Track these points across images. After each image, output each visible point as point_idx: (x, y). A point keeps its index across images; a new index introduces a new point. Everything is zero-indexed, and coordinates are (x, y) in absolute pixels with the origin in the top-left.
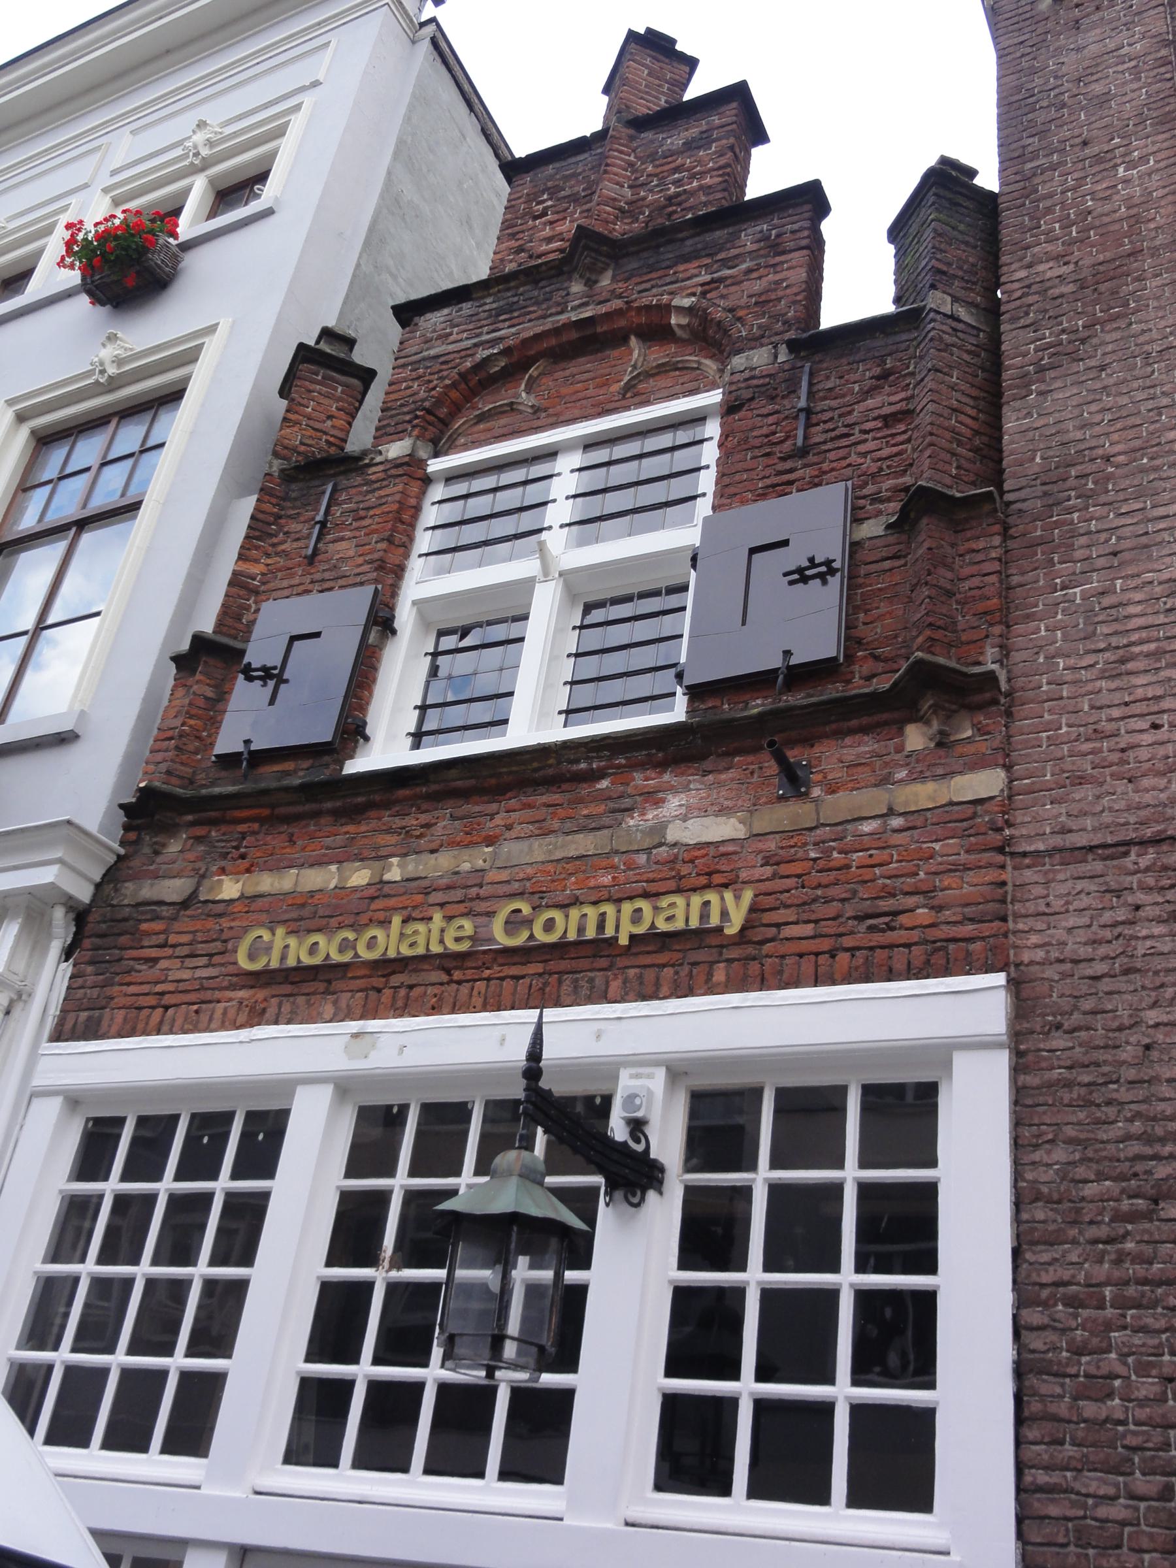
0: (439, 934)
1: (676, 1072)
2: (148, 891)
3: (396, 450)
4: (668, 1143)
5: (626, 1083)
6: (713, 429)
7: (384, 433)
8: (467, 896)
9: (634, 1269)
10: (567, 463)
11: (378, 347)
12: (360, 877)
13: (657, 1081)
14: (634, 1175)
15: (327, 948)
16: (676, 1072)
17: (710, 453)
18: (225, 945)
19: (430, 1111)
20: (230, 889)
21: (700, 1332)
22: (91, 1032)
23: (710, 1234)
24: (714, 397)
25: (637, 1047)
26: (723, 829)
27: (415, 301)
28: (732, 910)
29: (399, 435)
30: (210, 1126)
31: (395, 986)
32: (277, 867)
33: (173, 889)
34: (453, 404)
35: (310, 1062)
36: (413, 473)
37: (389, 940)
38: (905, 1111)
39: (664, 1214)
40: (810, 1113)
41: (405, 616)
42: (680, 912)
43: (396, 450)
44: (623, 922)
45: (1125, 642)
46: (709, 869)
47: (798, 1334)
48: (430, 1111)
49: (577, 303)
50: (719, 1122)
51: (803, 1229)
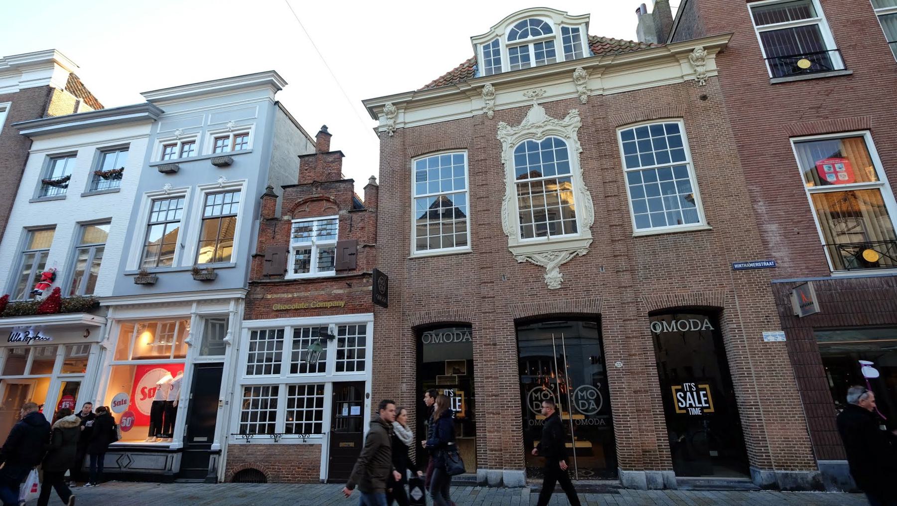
0: (302, 305)
1: (336, 324)
2: (255, 296)
3: (286, 218)
4: (336, 333)
5: (330, 326)
6: (337, 221)
7: (284, 214)
8: (306, 299)
9: (332, 348)
10: (315, 224)
11: (278, 191)
12: (290, 296)
13: (333, 326)
14: (332, 337)
15: (287, 307)
16: (336, 324)
17: (337, 226)
18: (269, 306)
19: (299, 387)
20: (269, 296)
21: (340, 354)
22: (250, 319)
23: (341, 341)
24: (337, 217)
25: (332, 321)
26: (341, 291)
27: (417, 387)
28: (342, 304)
29: (286, 214)
30: (272, 332)
31: (297, 312)
32: (277, 293)
33: (259, 296)
34: (294, 209)
35: (288, 323)
36: (289, 223)
37: (296, 306)
38: (363, 329)
39: (336, 341)
40: (352, 329)
41: (291, 249)
42: (336, 303)
43: (286, 218)
44: (329, 304)
45: (25, 77)
46: (338, 297)
47: (351, 355)
48: (299, 387)
49: (316, 193)
50: (342, 330)
51: (351, 342)
